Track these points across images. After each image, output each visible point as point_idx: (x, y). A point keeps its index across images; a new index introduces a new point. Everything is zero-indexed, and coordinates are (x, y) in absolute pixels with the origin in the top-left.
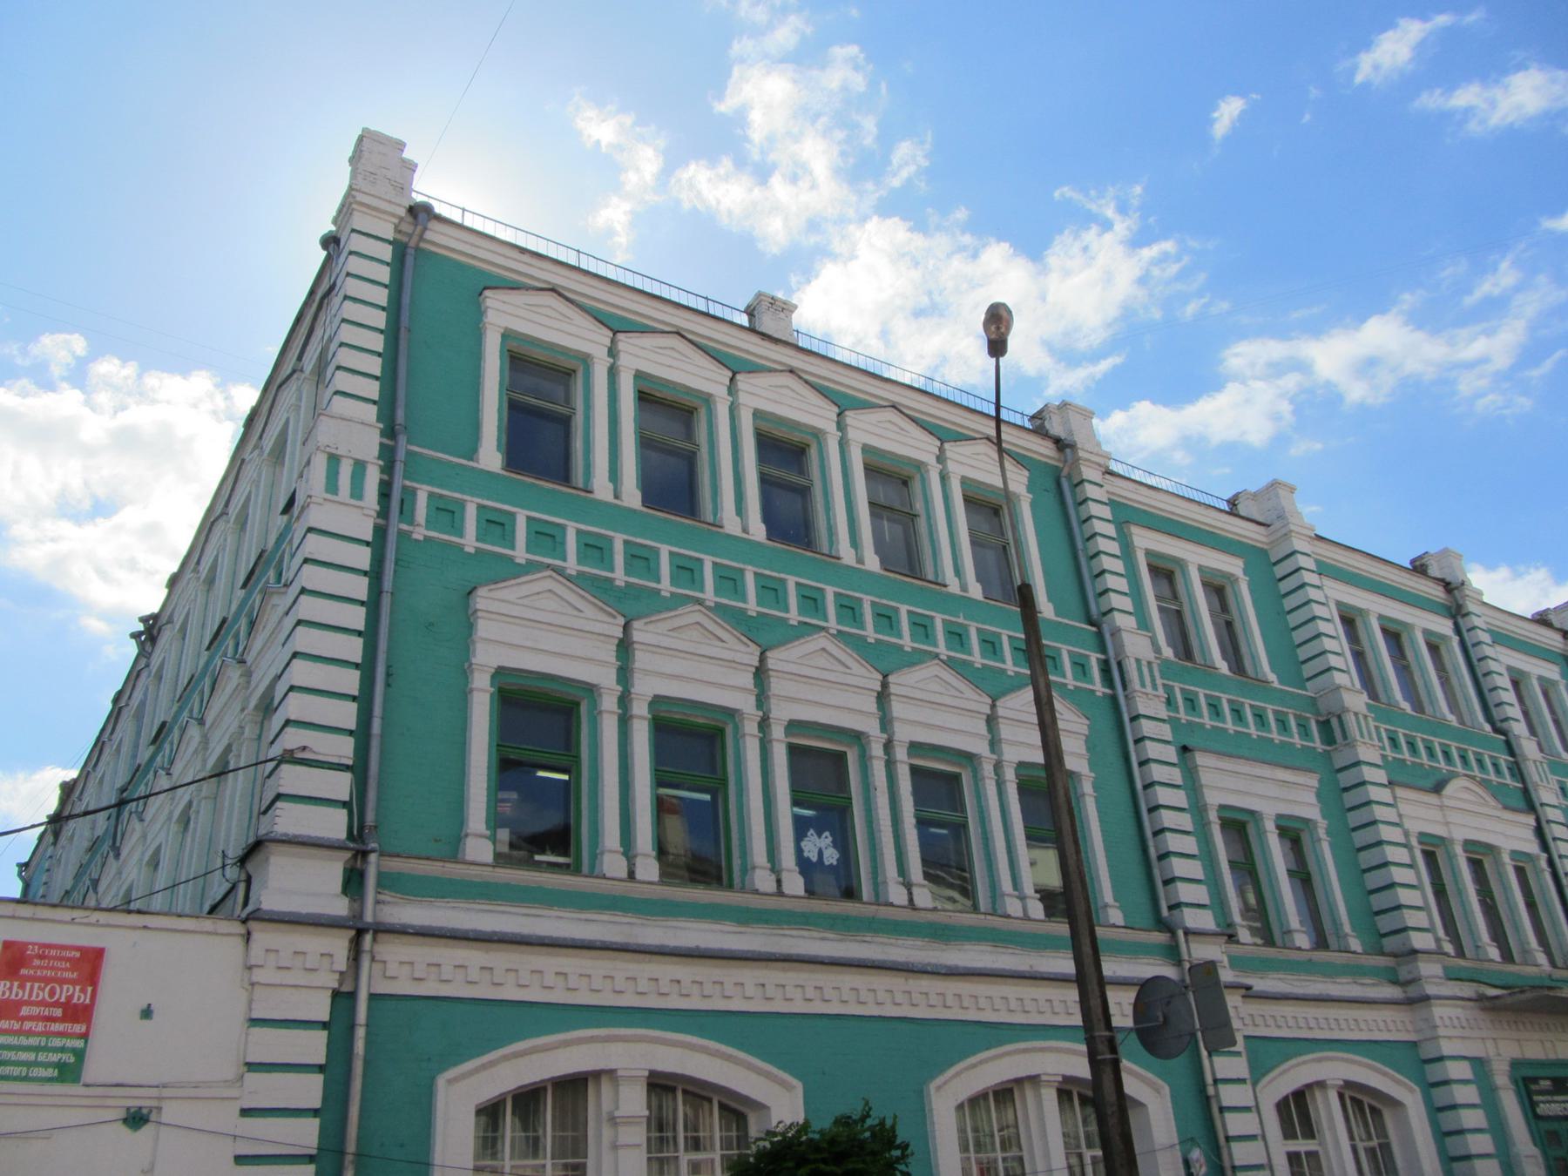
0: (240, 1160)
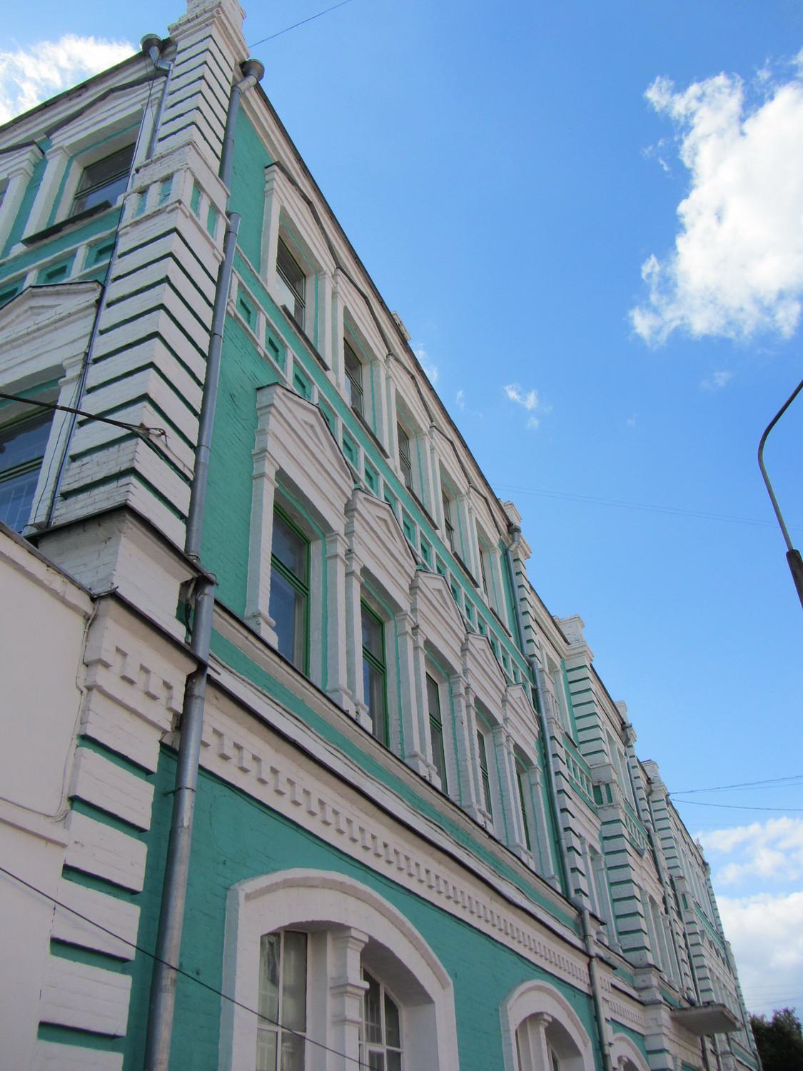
0: (60, 945)
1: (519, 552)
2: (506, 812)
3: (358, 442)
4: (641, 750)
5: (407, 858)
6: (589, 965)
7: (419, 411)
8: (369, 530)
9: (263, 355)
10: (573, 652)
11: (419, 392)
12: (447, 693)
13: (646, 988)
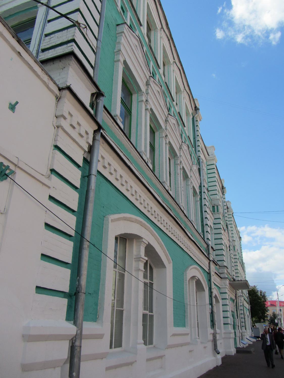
1: (198, 118)
2: (188, 209)
3: (151, 59)
4: (228, 197)
5: (161, 218)
6: (209, 263)
7: (170, 55)
8: (153, 94)
9: (119, 11)
10: (210, 159)
11: (171, 46)
12: (174, 163)
13: (223, 273)
